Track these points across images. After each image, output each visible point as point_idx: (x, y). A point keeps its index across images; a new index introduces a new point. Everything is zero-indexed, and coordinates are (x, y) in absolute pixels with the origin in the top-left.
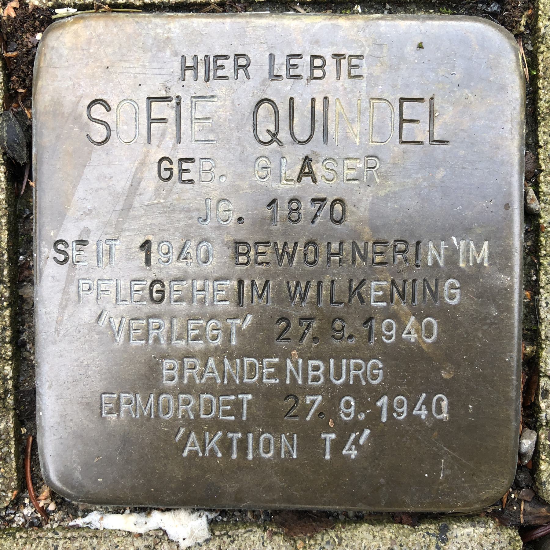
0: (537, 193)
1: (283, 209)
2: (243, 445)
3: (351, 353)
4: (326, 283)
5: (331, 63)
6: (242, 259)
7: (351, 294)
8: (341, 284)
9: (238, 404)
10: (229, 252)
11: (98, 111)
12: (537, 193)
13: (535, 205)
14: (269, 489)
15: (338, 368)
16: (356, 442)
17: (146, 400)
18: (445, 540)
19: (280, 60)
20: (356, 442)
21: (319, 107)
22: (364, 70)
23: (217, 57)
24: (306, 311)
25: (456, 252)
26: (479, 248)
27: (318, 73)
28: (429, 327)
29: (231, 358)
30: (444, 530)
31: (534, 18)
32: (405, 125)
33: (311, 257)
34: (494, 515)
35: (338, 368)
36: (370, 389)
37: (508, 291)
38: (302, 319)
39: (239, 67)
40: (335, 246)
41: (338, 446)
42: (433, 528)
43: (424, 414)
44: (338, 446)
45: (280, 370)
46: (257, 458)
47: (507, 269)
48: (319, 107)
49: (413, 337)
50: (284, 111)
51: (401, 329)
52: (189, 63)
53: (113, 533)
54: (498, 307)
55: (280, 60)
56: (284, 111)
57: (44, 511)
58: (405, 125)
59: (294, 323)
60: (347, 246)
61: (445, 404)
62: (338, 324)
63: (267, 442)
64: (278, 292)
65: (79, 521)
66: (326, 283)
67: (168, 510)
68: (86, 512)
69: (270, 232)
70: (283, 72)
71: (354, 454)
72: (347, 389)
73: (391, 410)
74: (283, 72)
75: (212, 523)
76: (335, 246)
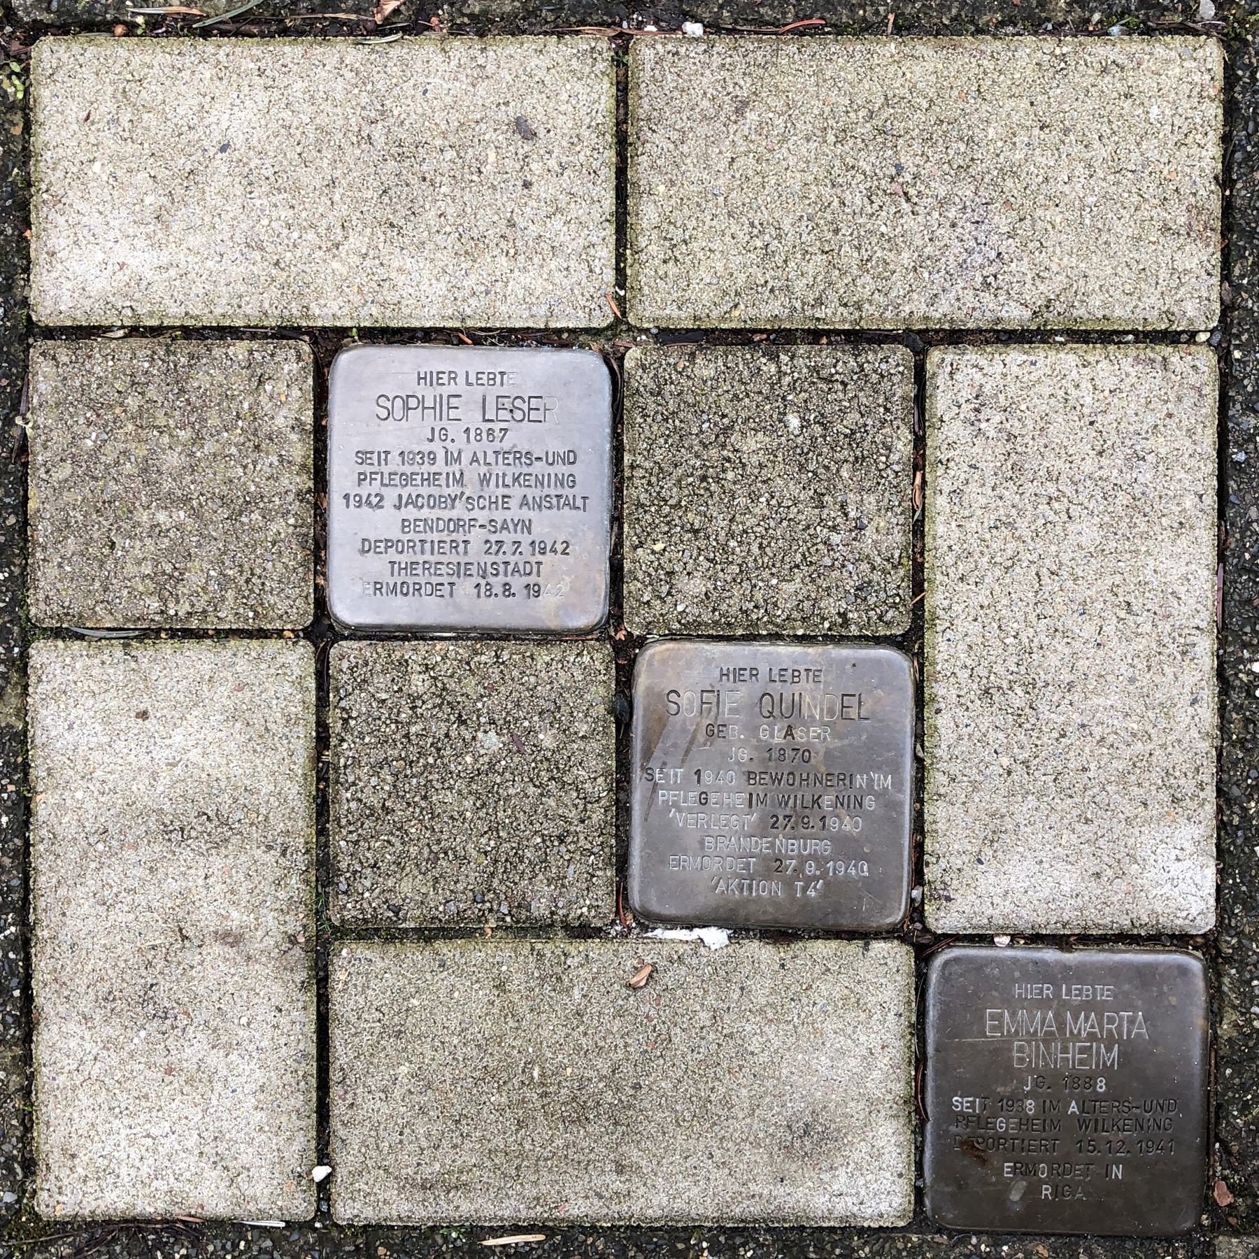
0: (923, 747)
1: (775, 755)
2: (750, 886)
3: (812, 837)
4: (799, 796)
5: (803, 673)
6: (752, 782)
7: (814, 802)
8: (808, 798)
9: (748, 864)
10: (745, 777)
11: (673, 697)
12: (923, 747)
13: (921, 754)
14: (765, 912)
15: (805, 845)
16: (815, 887)
17: (695, 861)
18: (867, 950)
19: (775, 671)
20: (815, 887)
21: (797, 698)
22: (822, 679)
23: (438, 373)
24: (788, 812)
25: (873, 780)
26: (886, 779)
27: (796, 679)
28: (857, 822)
29: (745, 837)
30: (867, 944)
31: (921, 648)
32: (900, 356)
33: (791, 782)
34: (898, 938)
35: (805, 845)
36: (823, 857)
37: (901, 804)
38: (785, 817)
39: (752, 675)
40: (805, 776)
41: (805, 889)
42: (861, 943)
43: (854, 872)
44: (805, 889)
45: (773, 845)
46: (758, 895)
47: (900, 791)
48: (797, 698)
49: (848, 828)
50: (777, 699)
51: (841, 824)
52: (725, 672)
53: (672, 941)
54: (897, 813)
55: (775, 671)
56: (777, 699)
57: (630, 929)
58: (900, 356)
59: (781, 818)
60: (812, 777)
61: (865, 867)
62: (806, 820)
63: (764, 887)
64: (772, 801)
65: (650, 934)
66: (799, 796)
67: (704, 927)
68: (654, 929)
69: (768, 767)
70: (777, 678)
71: (813, 894)
72: (811, 858)
73: (835, 869)
74: (777, 678)
75: (729, 938)
76: (805, 776)
